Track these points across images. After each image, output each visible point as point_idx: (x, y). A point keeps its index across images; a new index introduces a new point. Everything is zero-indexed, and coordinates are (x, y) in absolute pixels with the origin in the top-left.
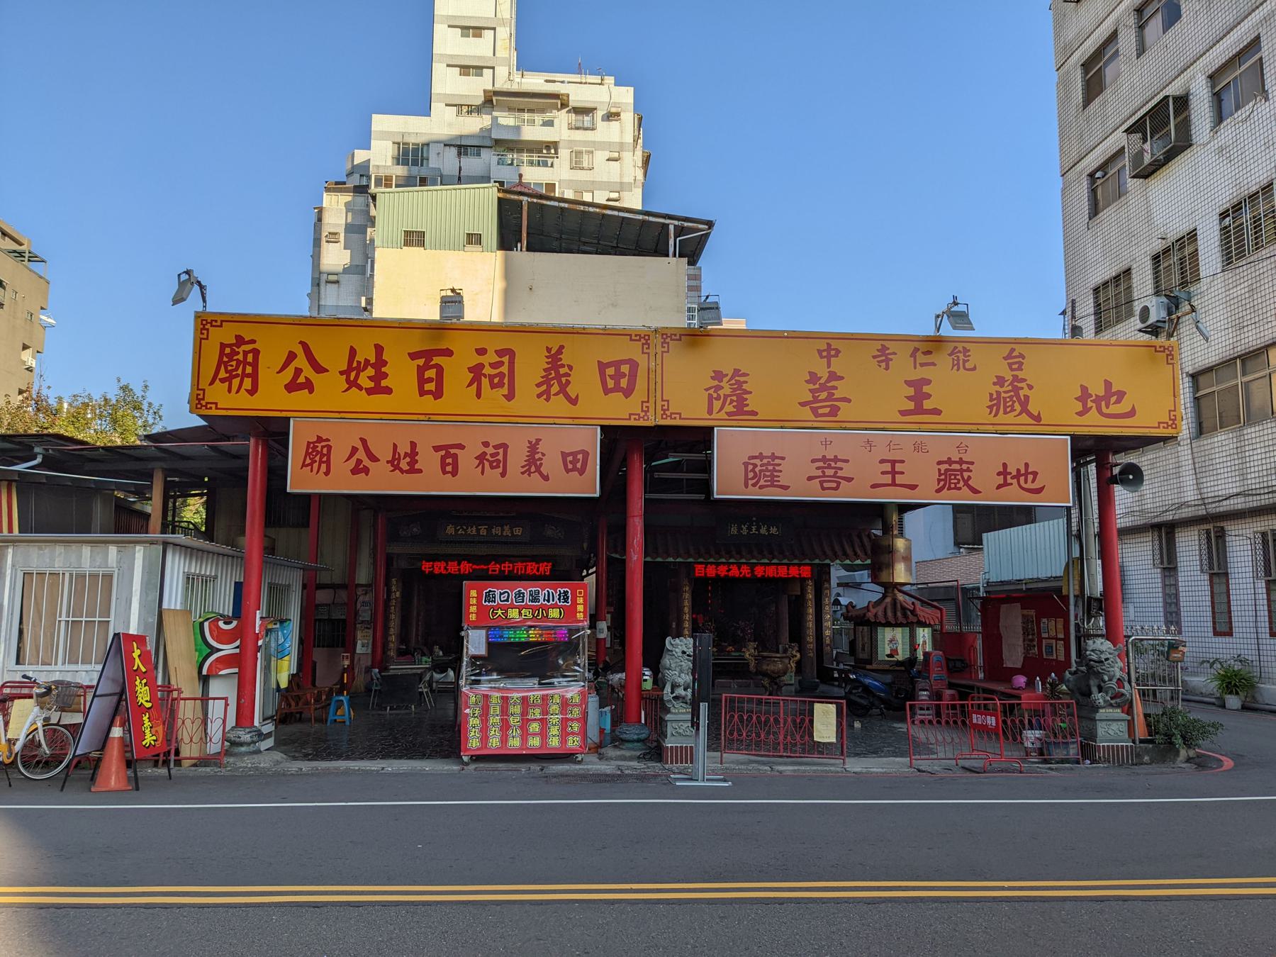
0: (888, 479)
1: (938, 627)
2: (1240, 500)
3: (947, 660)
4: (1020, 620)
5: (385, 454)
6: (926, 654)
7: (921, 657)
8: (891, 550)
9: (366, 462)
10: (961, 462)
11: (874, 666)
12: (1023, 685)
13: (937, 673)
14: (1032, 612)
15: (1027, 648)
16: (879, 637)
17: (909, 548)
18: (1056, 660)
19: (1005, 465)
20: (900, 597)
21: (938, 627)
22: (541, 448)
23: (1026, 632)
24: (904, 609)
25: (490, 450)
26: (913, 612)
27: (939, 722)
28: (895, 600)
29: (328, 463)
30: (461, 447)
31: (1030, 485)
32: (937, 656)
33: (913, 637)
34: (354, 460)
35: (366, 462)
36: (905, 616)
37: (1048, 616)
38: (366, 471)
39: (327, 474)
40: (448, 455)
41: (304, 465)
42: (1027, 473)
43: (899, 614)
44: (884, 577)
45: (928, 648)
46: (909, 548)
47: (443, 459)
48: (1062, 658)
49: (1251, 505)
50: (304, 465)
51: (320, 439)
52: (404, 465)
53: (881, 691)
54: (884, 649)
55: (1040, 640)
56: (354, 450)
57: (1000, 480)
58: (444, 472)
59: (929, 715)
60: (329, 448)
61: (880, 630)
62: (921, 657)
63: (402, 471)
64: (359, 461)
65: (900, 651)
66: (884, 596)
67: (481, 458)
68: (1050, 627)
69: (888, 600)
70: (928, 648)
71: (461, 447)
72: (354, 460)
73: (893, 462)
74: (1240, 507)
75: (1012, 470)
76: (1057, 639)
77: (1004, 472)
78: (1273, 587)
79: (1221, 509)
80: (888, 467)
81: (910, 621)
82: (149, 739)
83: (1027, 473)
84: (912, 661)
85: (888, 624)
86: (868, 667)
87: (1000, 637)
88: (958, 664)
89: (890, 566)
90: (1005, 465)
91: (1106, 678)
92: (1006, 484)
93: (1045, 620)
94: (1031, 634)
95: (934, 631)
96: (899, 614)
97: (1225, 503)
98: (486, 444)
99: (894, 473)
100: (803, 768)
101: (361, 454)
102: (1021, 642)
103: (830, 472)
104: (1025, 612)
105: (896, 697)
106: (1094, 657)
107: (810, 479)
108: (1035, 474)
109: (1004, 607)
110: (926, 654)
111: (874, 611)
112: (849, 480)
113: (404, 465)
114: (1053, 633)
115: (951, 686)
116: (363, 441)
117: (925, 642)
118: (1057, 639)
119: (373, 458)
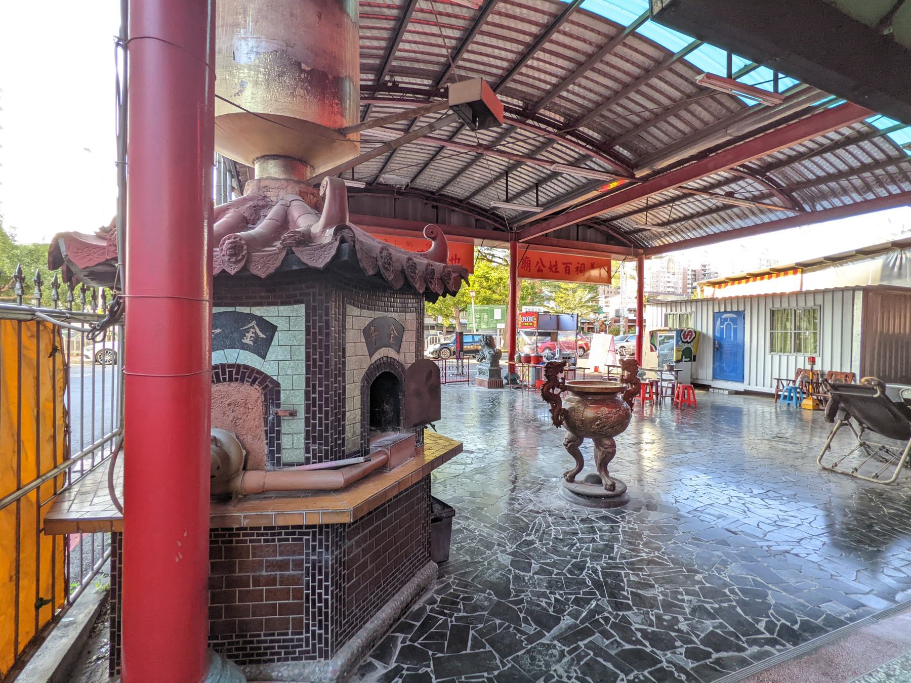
67: (577, 268)
101: (540, 264)
119: (544, 266)
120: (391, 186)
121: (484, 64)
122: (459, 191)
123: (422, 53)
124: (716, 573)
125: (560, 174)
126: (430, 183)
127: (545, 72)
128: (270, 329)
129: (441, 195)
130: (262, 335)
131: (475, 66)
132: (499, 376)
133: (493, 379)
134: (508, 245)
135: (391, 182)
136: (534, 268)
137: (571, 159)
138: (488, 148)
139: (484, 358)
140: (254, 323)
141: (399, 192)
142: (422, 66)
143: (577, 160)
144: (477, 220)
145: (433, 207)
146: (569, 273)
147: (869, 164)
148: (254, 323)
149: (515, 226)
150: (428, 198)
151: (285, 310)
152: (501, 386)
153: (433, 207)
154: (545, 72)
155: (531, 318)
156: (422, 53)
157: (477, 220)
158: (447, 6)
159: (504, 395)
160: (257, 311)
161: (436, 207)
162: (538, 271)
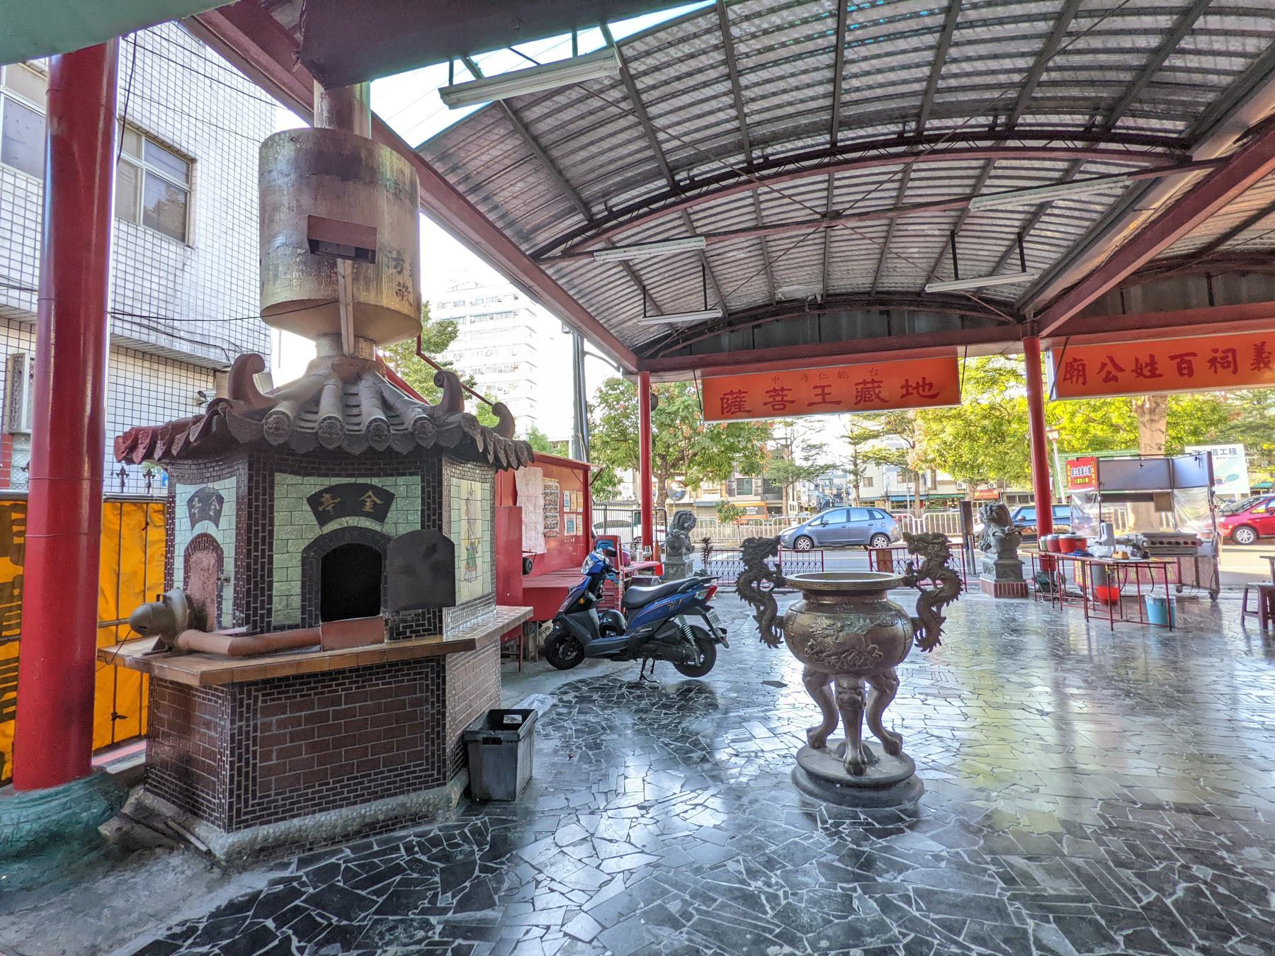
0: (819, 399)
5: (1129, 365)
9: (1115, 373)
10: (873, 382)
19: (907, 381)
22: (1267, 349)
25: (1219, 355)
29: (1084, 375)
30: (1194, 355)
31: (926, 393)
34: (1104, 372)
35: (1115, 373)
38: (1115, 379)
39: (1084, 383)
40: (1183, 361)
41: (1065, 379)
42: (923, 386)
47: (1179, 365)
50: (1065, 379)
51: (1075, 360)
52: (1146, 372)
56: (1104, 365)
57: (904, 391)
58: (1181, 374)
60: (1084, 365)
63: (1146, 377)
64: (1109, 373)
67: (1213, 361)
71: (1194, 355)
72: (1104, 372)
73: (823, 387)
75: (912, 383)
77: (906, 386)
80: (819, 391)
82: (833, 685)
83: (923, 386)
90: (907, 381)
92: (908, 394)
98: (1216, 351)
99: (823, 394)
101: (1110, 367)
103: (779, 398)
107: (765, 404)
108: (931, 385)
112: (792, 402)
113: (1146, 372)
114: (574, 508)
116: (1111, 359)
119: (1121, 370)
120: (802, 301)
121: (768, 109)
122: (898, 279)
123: (697, 130)
124: (1024, 912)
125: (1048, 204)
126: (854, 281)
127: (892, 69)
128: (388, 498)
129: (878, 293)
130: (379, 502)
131: (779, 112)
132: (1019, 574)
133: (1003, 581)
134: (1021, 345)
135: (799, 295)
136: (1094, 376)
137: (1057, 175)
138: (899, 208)
139: (989, 546)
140: (370, 493)
141: (813, 304)
142: (879, 106)
143: (1067, 171)
144: (962, 317)
145: (881, 313)
146: (1191, 374)
147: (1035, 65)
148: (370, 493)
149: (1029, 311)
150: (869, 303)
151: (401, 480)
152: (1023, 593)
153: (881, 313)
154: (892, 69)
155: (1086, 469)
156: (697, 130)
157: (962, 317)
158: (677, 67)
159: (1033, 613)
160: (375, 481)
161: (888, 313)
162: (1106, 380)
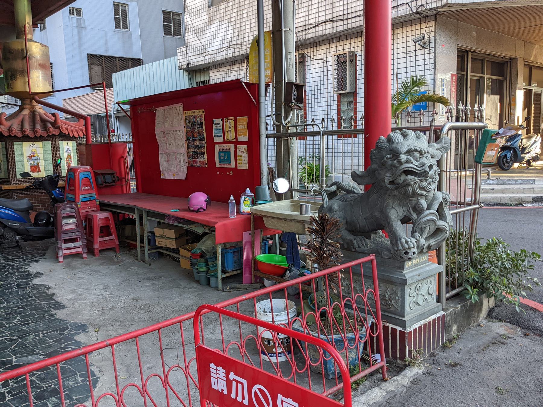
1: (83, 141)
2: (328, 26)
3: (96, 174)
4: (182, 124)
6: (71, 170)
7: (64, 173)
8: (25, 56)
11: (12, 186)
12: (204, 205)
13: (85, 194)
14: (200, 113)
15: (192, 158)
16: (17, 153)
17: (46, 55)
18: (235, 169)
20: (40, 109)
21: (83, 141)
23: (190, 137)
24: (44, 121)
26: (55, 124)
27: (90, 251)
28: (33, 113)
32: (85, 172)
33: (55, 151)
36: (45, 128)
37: (223, 116)
43: (38, 127)
44: (19, 86)
45: (74, 163)
46: (46, 55)
48: (244, 165)
49: (338, 29)
53: (15, 219)
54: (23, 165)
55: (211, 145)
59: (78, 246)
61: (17, 145)
62: (64, 173)
65: (42, 167)
66: (22, 109)
68: (229, 128)
69: (26, 112)
70: (74, 163)
74: (328, 32)
76: (237, 143)
78: (2, 175)
79: (311, 36)
81: (49, 132)
84: (53, 180)
85: (26, 138)
86: (5, 187)
87: (156, 145)
88: (109, 179)
89: (26, 72)
91: (424, 203)
93: (219, 121)
94: (199, 138)
95: (79, 145)
96: (38, 127)
97: (314, 30)
100: (105, 127)
102: (183, 149)
104: (190, 113)
105: (36, 224)
106: (414, 165)
109: (160, 112)
110: (71, 170)
111: (8, 124)
114: (231, 136)
115: (103, 207)
117: (69, 157)
118: (237, 143)
